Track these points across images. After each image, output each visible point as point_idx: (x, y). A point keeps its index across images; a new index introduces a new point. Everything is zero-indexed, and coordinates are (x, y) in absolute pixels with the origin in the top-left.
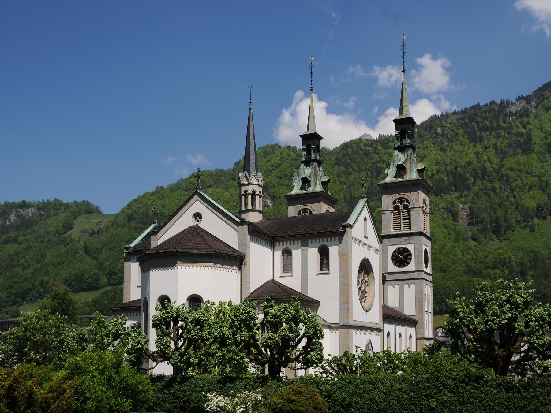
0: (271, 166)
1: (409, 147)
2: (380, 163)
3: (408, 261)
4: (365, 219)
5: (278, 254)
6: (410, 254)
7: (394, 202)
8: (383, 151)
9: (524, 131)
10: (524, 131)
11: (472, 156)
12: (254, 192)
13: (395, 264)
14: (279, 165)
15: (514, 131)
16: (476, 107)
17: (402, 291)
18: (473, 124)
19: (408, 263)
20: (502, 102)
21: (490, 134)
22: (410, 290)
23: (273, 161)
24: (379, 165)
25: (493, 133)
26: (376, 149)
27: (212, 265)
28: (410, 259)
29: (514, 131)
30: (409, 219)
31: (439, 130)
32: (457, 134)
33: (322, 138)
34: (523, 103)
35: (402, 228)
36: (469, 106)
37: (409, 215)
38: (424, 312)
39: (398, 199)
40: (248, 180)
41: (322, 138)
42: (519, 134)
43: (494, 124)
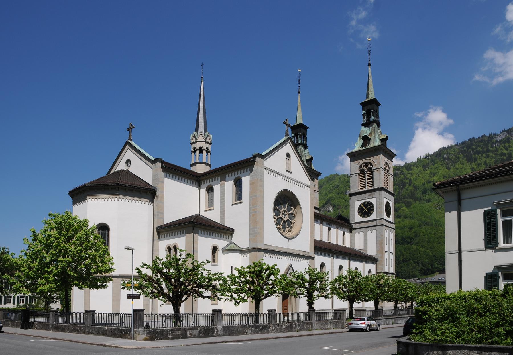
0: (333, 187)
1: (373, 122)
2: (404, 179)
3: (371, 212)
4: (288, 155)
5: (204, 191)
6: (373, 206)
7: (360, 167)
8: (407, 172)
9: (506, 152)
10: (506, 152)
11: (469, 170)
12: (201, 148)
13: (361, 216)
14: (338, 186)
15: (499, 152)
16: (472, 140)
17: (365, 236)
18: (470, 150)
19: (371, 214)
20: (490, 135)
21: (482, 156)
22: (372, 235)
23: (334, 184)
24: (404, 181)
25: (484, 155)
26: (402, 171)
27: (118, 196)
28: (373, 210)
29: (499, 152)
30: (372, 178)
31: (445, 156)
32: (458, 158)
33: (308, 128)
34: (506, 134)
35: (367, 186)
36: (467, 139)
37: (373, 176)
38: (384, 252)
39: (363, 163)
40: (196, 139)
41: (308, 128)
42: (504, 154)
43: (485, 149)
